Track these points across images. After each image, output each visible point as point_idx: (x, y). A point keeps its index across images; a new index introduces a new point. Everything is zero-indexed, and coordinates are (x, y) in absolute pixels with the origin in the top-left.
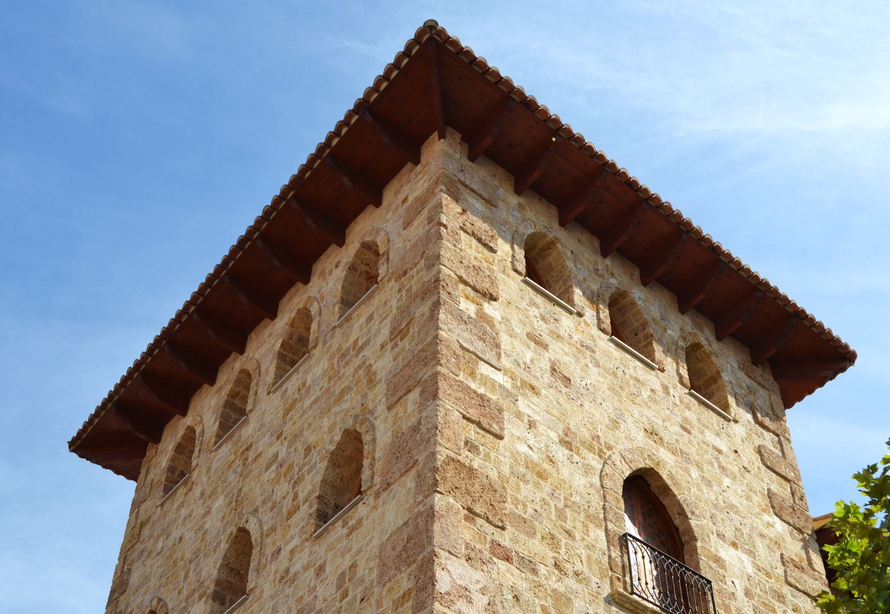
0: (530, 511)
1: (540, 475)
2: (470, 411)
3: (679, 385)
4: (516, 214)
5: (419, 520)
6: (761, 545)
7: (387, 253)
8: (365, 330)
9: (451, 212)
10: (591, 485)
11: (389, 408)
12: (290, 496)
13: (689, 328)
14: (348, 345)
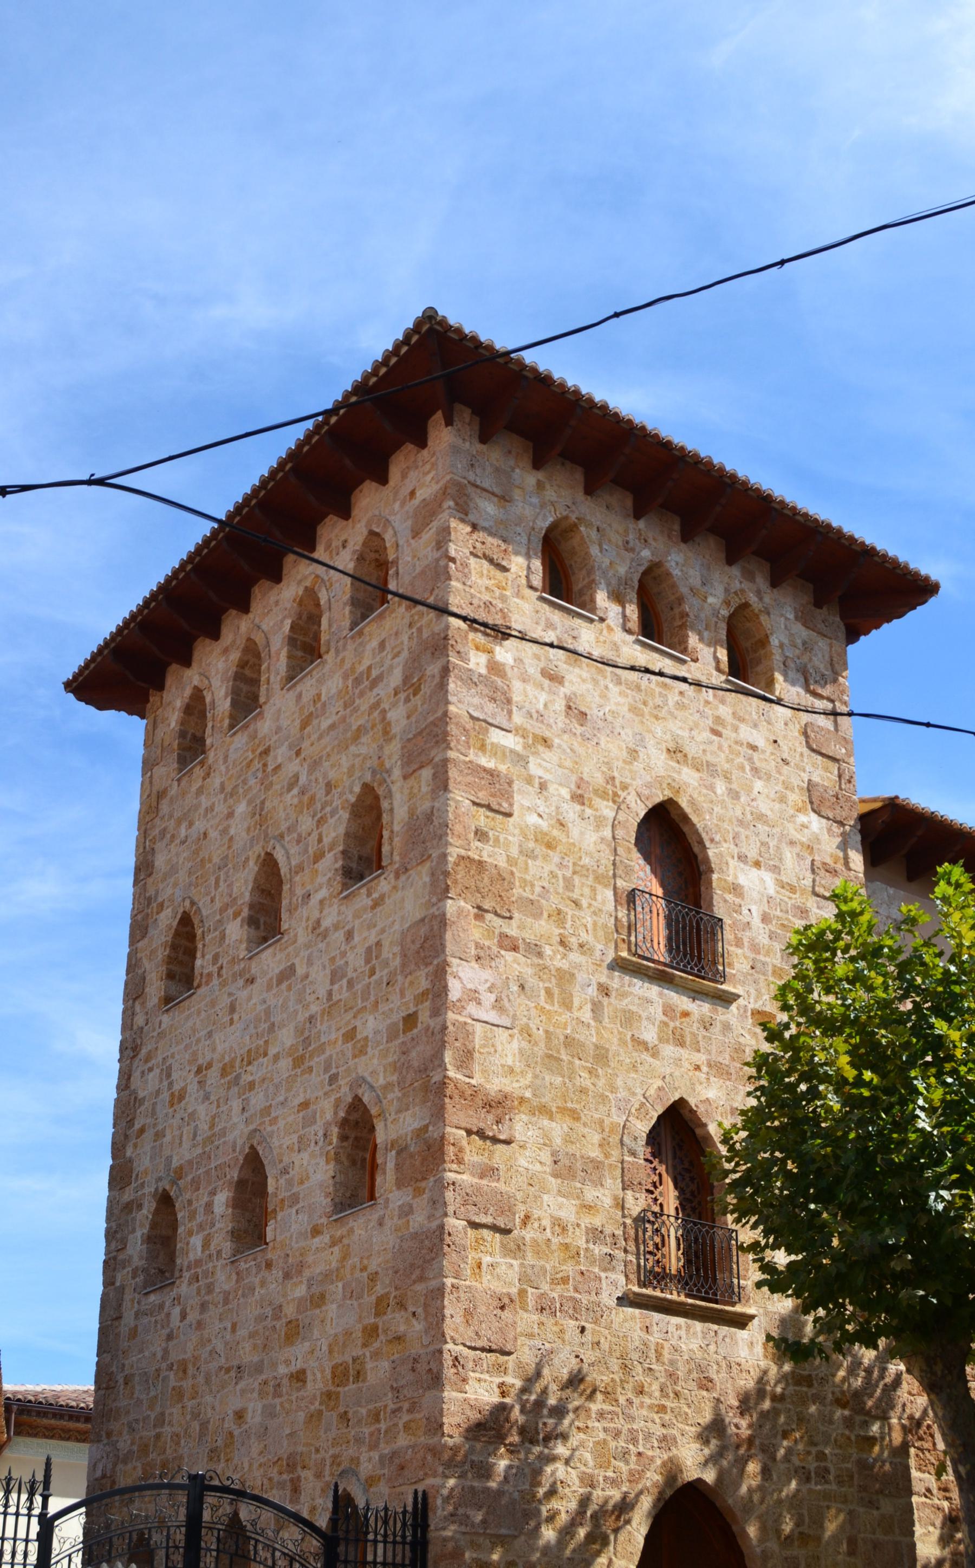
0: (538, 889)
1: (549, 846)
2: (480, 794)
4: (535, 500)
6: (789, 855)
7: (395, 562)
9: (462, 538)
11: (405, 777)
12: (315, 836)
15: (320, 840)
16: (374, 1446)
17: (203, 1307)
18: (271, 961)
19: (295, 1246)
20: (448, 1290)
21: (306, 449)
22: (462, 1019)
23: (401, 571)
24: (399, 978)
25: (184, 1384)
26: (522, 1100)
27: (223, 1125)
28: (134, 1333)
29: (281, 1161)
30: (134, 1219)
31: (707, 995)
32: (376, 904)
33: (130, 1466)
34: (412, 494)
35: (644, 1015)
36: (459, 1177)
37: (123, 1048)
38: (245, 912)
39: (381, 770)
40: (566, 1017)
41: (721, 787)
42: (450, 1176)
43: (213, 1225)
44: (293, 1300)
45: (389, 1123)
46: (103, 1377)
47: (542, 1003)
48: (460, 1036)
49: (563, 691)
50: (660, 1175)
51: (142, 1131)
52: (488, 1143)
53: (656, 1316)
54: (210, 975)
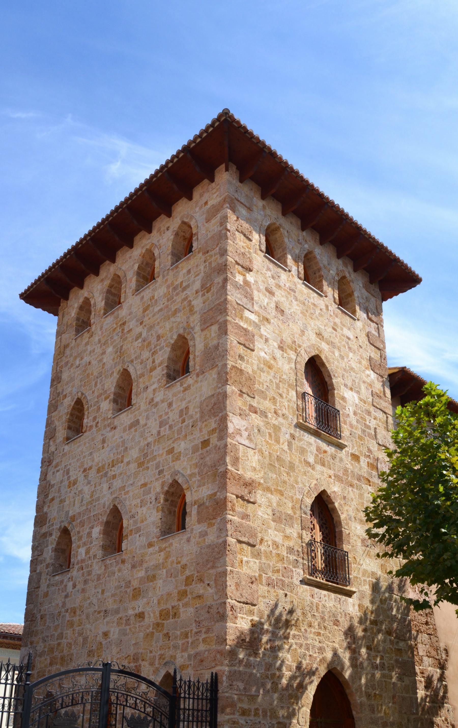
0: (265, 387)
1: (270, 367)
2: (241, 339)
3: (333, 303)
4: (262, 213)
5: (220, 396)
7: (197, 234)
8: (186, 278)
9: (233, 222)
10: (291, 368)
11: (202, 330)
12: (151, 360)
13: (341, 268)
14: (177, 283)
15: (154, 362)
16: (184, 650)
17: (86, 582)
18: (126, 418)
19: (138, 552)
20: (228, 573)
21: (154, 179)
22: (234, 442)
23: (199, 238)
24: (199, 423)
25: (74, 619)
26: (260, 484)
27: (98, 495)
28: (46, 595)
29: (130, 512)
30: (47, 541)
31: (333, 444)
32: (185, 390)
33: (43, 658)
34: (206, 203)
35: (309, 450)
36: (233, 518)
37: (43, 462)
38: (112, 397)
39: (189, 328)
40: (277, 447)
41: (337, 354)
42: (229, 517)
43: (91, 543)
44: (137, 578)
45: (193, 492)
46: (29, 616)
47: (267, 440)
48: (233, 450)
49: (274, 299)
50: (314, 525)
51: (53, 499)
52: (245, 502)
53: (316, 590)
54: (91, 427)
